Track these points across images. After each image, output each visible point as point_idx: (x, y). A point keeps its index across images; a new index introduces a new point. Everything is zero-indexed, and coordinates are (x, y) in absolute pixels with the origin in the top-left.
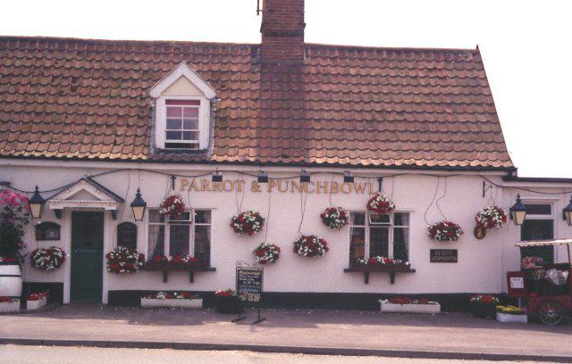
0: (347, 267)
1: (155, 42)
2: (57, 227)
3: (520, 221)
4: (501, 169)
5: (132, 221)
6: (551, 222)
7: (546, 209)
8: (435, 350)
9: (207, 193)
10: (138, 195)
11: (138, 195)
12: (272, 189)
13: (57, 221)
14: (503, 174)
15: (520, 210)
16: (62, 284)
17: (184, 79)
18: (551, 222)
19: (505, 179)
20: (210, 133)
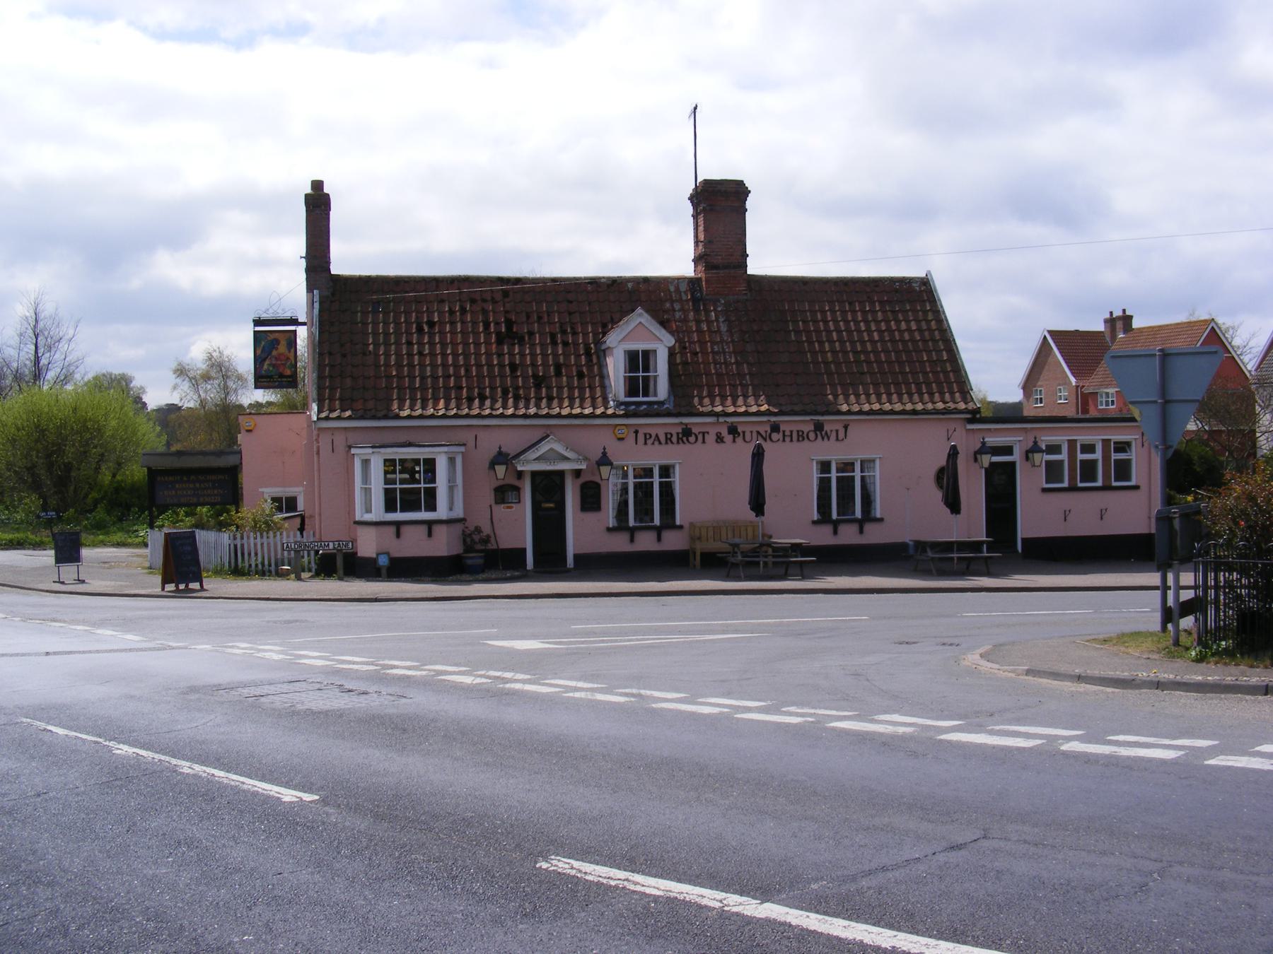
0: (755, 514)
1: (574, 278)
2: (517, 489)
3: (986, 464)
4: (966, 411)
5: (597, 479)
6: (1013, 464)
7: (1008, 450)
8: (607, 591)
9: (670, 445)
10: (604, 454)
11: (604, 454)
12: (737, 440)
13: (516, 483)
14: (969, 416)
15: (986, 453)
16: (524, 550)
17: (641, 325)
18: (1013, 464)
19: (971, 421)
20: (950, 452)
